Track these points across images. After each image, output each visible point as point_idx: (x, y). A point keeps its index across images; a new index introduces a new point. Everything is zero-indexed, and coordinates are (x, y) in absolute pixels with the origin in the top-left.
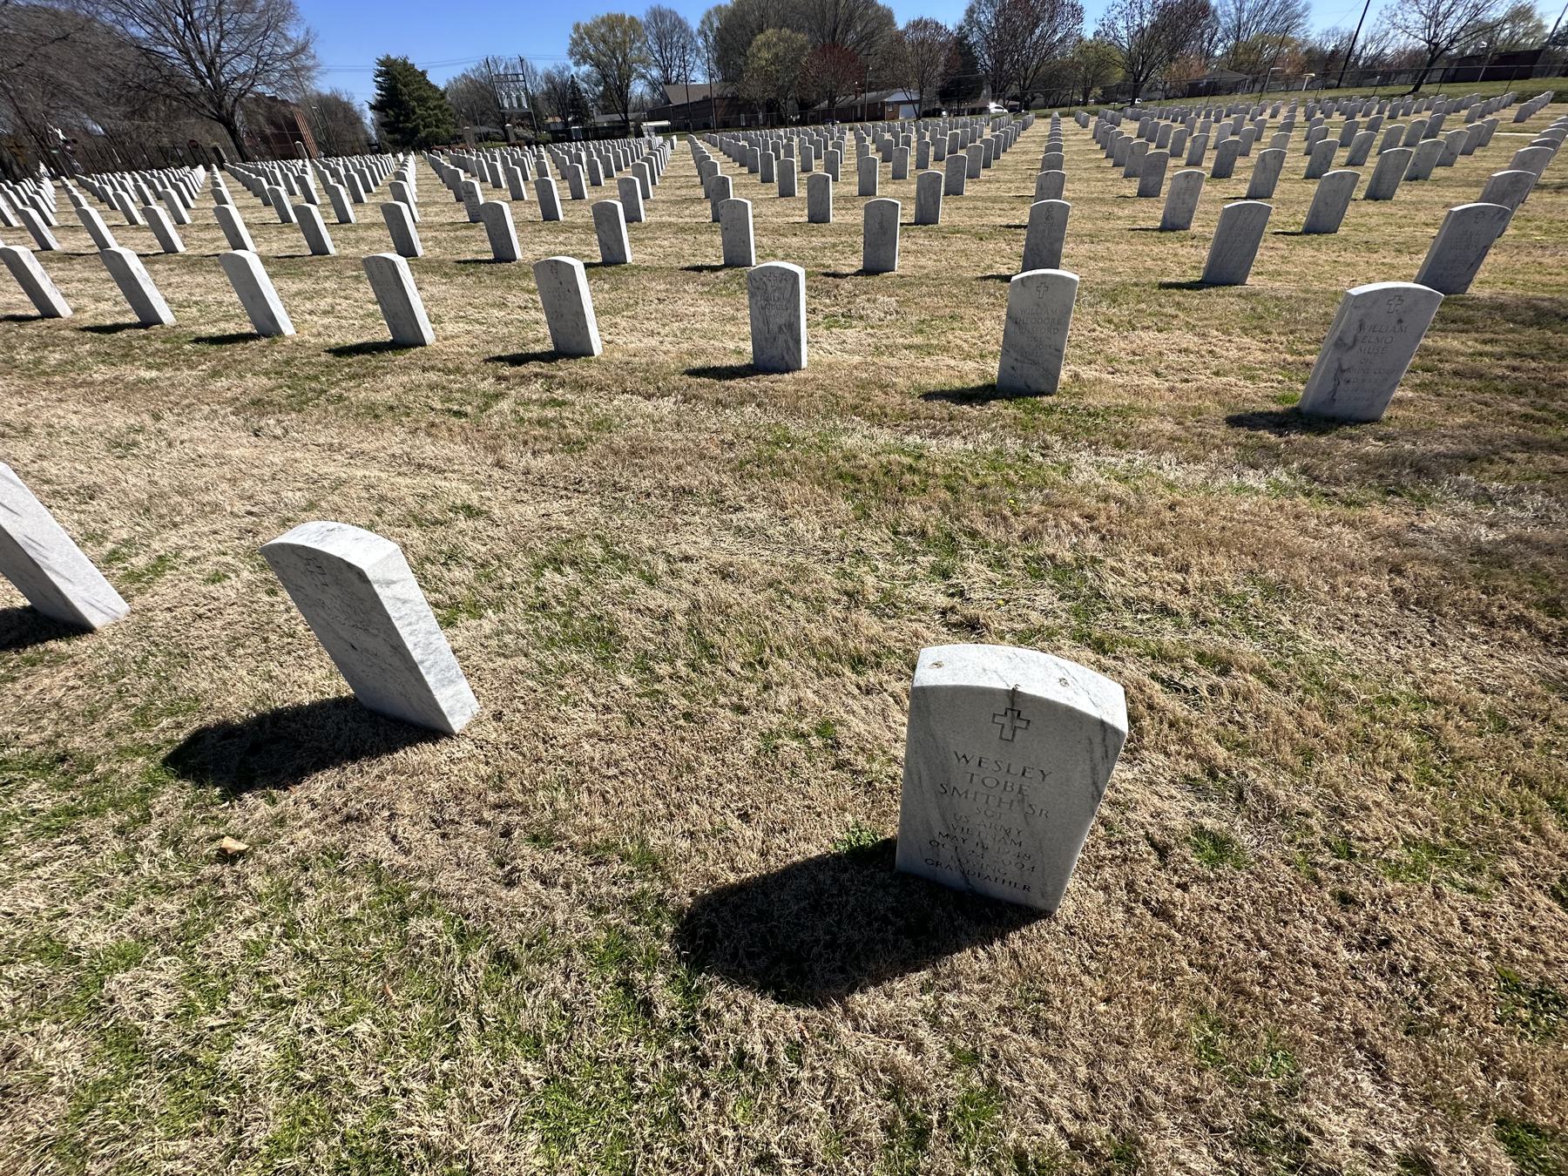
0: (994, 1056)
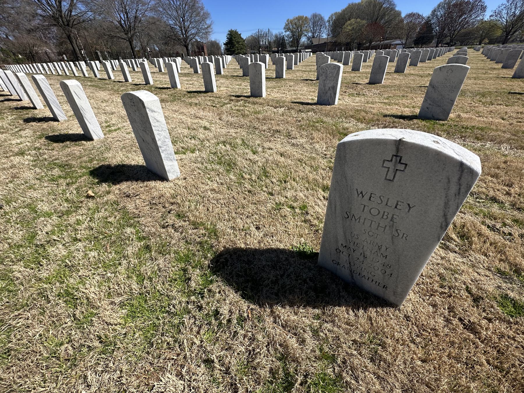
0: (344, 362)
